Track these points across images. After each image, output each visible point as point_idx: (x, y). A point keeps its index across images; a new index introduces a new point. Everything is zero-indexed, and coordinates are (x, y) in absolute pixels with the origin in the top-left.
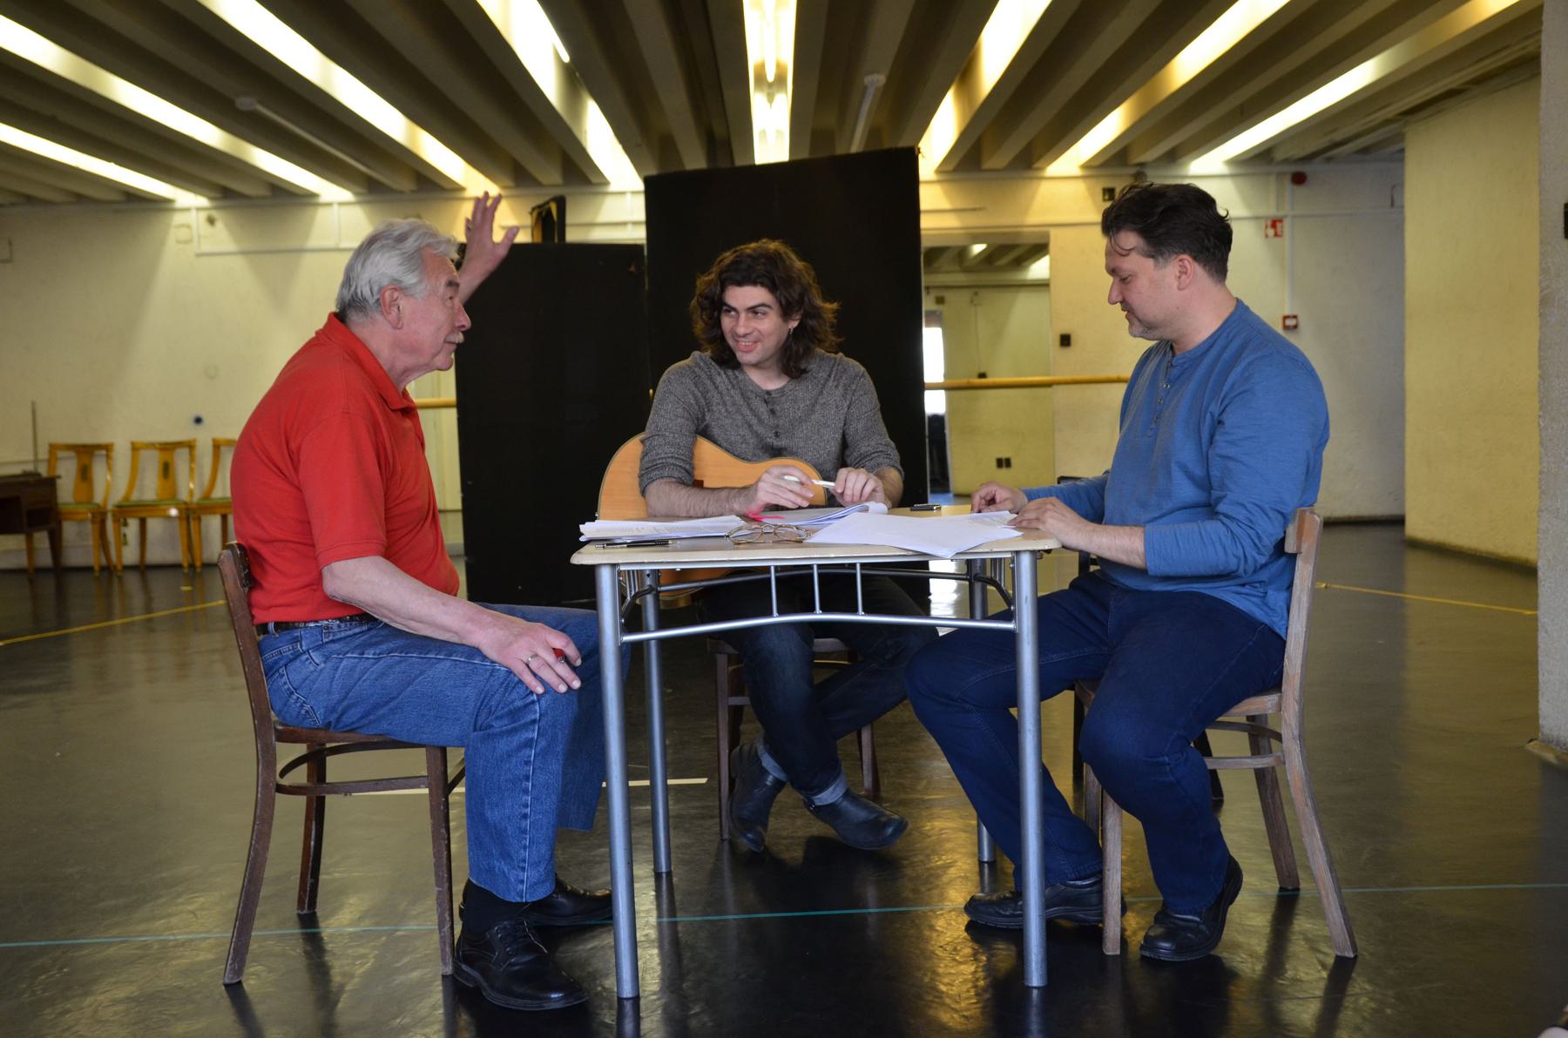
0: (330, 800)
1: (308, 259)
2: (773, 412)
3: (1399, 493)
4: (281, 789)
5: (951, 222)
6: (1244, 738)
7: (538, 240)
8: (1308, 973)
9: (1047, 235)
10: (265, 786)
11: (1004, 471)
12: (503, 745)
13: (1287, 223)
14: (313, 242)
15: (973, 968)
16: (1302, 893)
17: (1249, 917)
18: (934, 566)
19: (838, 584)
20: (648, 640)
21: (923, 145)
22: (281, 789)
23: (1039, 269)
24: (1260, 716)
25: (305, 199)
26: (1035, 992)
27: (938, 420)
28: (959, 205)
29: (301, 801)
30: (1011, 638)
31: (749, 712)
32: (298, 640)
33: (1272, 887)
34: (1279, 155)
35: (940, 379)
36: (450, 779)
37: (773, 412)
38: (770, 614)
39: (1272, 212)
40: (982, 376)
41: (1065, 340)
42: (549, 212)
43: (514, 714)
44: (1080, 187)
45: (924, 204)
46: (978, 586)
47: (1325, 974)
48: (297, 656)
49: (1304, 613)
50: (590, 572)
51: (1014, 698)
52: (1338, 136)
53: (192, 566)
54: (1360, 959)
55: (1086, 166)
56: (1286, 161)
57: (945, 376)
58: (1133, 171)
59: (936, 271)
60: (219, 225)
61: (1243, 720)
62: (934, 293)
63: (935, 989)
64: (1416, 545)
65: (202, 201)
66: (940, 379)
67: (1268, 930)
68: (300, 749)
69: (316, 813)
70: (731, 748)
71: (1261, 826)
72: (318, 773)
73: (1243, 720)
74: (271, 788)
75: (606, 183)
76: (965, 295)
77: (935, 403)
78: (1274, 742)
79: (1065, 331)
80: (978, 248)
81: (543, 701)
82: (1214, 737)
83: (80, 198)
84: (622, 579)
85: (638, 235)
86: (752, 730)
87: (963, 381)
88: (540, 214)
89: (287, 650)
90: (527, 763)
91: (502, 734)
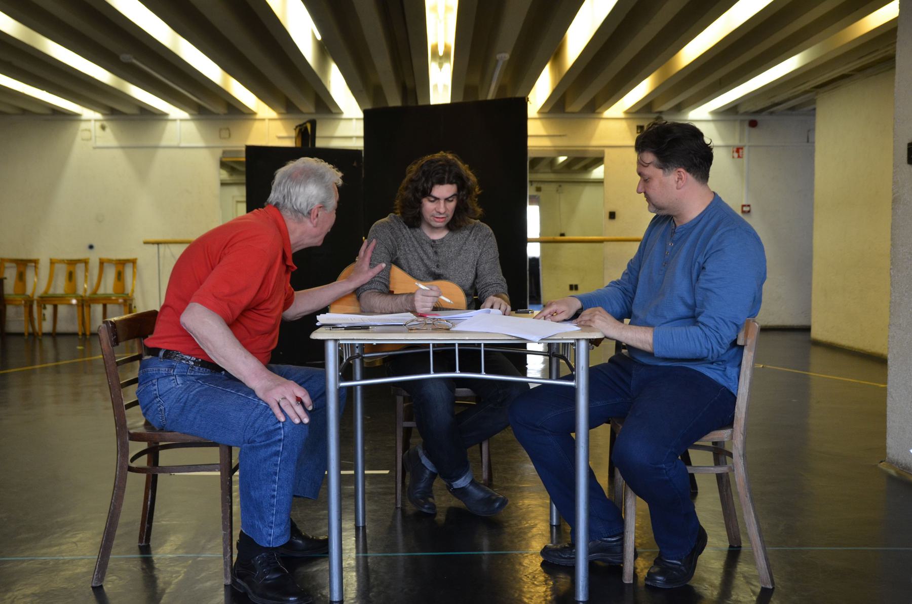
0: (161, 477)
1: (161, 153)
2: (436, 253)
3: (807, 310)
4: (131, 469)
5: (546, 143)
6: (710, 455)
7: (299, 145)
9: (603, 152)
10: (121, 467)
12: (263, 453)
13: (745, 150)
14: (164, 143)
16: (743, 549)
17: (711, 562)
18: (530, 347)
19: (470, 355)
20: (356, 386)
21: (531, 96)
22: (131, 469)
23: (598, 173)
24: (720, 442)
25: (159, 116)
27: (535, 261)
28: (552, 133)
29: (143, 477)
30: (573, 391)
31: (415, 431)
33: (725, 545)
34: (742, 109)
35: (537, 236)
36: (233, 466)
37: (436, 253)
38: (428, 372)
39: (737, 143)
40: (562, 235)
41: (612, 215)
42: (306, 129)
44: (624, 125)
45: (530, 131)
46: (554, 360)
47: (755, 598)
48: (168, 375)
49: (748, 373)
50: (322, 343)
51: (573, 427)
52: (777, 100)
53: (84, 334)
55: (627, 112)
56: (746, 113)
57: (540, 235)
58: (655, 116)
59: (537, 172)
60: (108, 130)
61: (710, 444)
62: (535, 185)
65: (98, 116)
66: (537, 236)
67: (722, 571)
68: (144, 446)
69: (152, 485)
70: (404, 451)
71: (720, 508)
72: (154, 460)
73: (710, 444)
74: (125, 468)
75: (341, 113)
76: (553, 187)
77: (533, 250)
78: (728, 458)
79: (612, 210)
80: (562, 159)
81: (286, 429)
82: (693, 454)
83: (24, 112)
84: (341, 349)
85: (359, 144)
86: (416, 441)
87: (551, 238)
88: (300, 130)
89: (163, 370)
90: (276, 465)
91: (261, 447)
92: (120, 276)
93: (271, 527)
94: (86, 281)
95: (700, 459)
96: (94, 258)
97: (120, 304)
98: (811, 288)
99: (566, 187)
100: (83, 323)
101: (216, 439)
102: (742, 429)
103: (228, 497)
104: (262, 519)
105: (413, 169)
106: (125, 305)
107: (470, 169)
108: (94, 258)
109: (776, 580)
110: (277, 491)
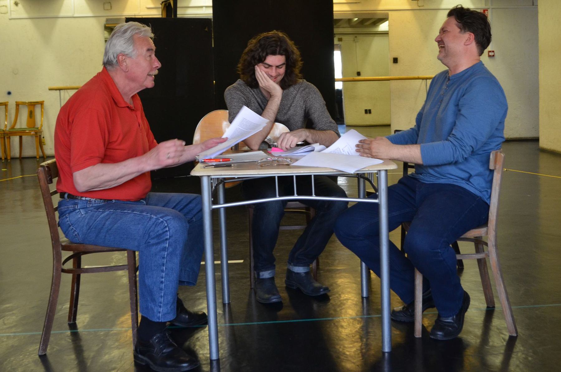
0: (83, 276)
1: (60, 20)
3: (536, 127)
4: (64, 271)
5: (346, 8)
7: (164, 16)
8: (498, 341)
9: (387, 15)
10: (57, 270)
11: (368, 115)
12: (154, 249)
14: (62, 14)
15: (360, 344)
16: (496, 309)
17: (475, 313)
19: (304, 183)
22: (64, 271)
23: (384, 27)
24: (479, 237)
26: (386, 354)
27: (339, 92)
29: (70, 276)
30: (376, 206)
32: (76, 204)
33: (484, 306)
38: (275, 196)
41: (395, 60)
42: (170, 4)
43: (159, 236)
46: (362, 180)
47: (505, 343)
48: (75, 210)
49: (497, 188)
50: (198, 179)
53: (6, 159)
54: (518, 337)
63: (344, 354)
64: (544, 151)
67: (482, 325)
68: (71, 253)
69: (76, 281)
71: (479, 279)
72: (78, 263)
74: (59, 270)
76: (351, 38)
77: (338, 86)
78: (485, 247)
85: (208, 13)
87: (351, 78)
88: (165, 4)
89: (71, 207)
90: (164, 258)
91: (153, 245)
92: (31, 114)
93: (160, 307)
94: (6, 119)
95: (466, 248)
96: (12, 101)
97: (32, 136)
98: (538, 110)
99: (360, 38)
100: (5, 151)
101: (124, 246)
102: (494, 227)
103: (134, 288)
104: (153, 300)
105: (252, 43)
106: (36, 137)
107: (296, 44)
108: (12, 101)
109: (519, 330)
110: (164, 278)
